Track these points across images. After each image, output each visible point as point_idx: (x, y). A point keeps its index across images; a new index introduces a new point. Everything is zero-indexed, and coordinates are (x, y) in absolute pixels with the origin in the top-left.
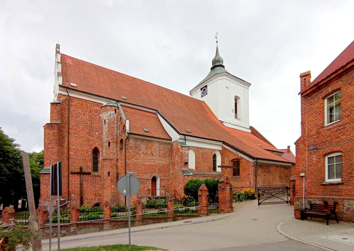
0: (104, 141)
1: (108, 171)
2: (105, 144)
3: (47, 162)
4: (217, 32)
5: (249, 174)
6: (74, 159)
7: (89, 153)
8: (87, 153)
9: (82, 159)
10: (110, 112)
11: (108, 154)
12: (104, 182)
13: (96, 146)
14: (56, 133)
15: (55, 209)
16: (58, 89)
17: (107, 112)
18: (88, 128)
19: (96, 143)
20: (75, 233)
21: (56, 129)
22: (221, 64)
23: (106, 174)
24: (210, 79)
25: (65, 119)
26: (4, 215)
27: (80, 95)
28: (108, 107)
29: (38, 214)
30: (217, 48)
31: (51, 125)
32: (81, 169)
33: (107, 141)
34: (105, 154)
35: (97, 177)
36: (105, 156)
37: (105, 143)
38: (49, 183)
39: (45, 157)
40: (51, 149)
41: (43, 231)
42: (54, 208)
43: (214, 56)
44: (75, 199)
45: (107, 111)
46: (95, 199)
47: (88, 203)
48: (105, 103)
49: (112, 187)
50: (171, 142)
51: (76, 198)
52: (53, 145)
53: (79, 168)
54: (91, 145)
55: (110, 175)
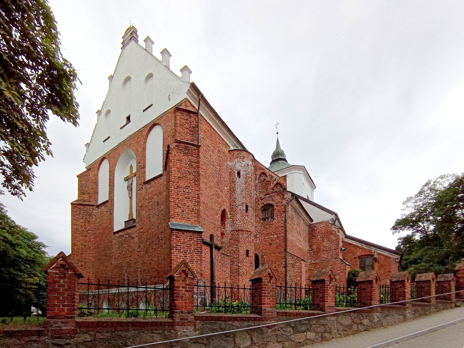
0: (238, 203)
1: (245, 249)
2: (239, 207)
3: (176, 210)
4: (277, 122)
5: (389, 272)
10: (247, 161)
12: (239, 264)
14: (195, 163)
16: (187, 90)
17: (244, 160)
19: (225, 203)
20: (380, 325)
21: (194, 155)
22: (281, 157)
23: (242, 252)
24: (283, 170)
26: (267, 283)
27: (211, 119)
28: (244, 153)
30: (278, 139)
31: (185, 147)
33: (242, 203)
34: (240, 222)
37: (239, 205)
38: (189, 249)
39: (173, 202)
40: (184, 188)
41: (336, 320)
43: (274, 149)
45: (242, 157)
50: (311, 223)
52: (190, 183)
53: (209, 236)
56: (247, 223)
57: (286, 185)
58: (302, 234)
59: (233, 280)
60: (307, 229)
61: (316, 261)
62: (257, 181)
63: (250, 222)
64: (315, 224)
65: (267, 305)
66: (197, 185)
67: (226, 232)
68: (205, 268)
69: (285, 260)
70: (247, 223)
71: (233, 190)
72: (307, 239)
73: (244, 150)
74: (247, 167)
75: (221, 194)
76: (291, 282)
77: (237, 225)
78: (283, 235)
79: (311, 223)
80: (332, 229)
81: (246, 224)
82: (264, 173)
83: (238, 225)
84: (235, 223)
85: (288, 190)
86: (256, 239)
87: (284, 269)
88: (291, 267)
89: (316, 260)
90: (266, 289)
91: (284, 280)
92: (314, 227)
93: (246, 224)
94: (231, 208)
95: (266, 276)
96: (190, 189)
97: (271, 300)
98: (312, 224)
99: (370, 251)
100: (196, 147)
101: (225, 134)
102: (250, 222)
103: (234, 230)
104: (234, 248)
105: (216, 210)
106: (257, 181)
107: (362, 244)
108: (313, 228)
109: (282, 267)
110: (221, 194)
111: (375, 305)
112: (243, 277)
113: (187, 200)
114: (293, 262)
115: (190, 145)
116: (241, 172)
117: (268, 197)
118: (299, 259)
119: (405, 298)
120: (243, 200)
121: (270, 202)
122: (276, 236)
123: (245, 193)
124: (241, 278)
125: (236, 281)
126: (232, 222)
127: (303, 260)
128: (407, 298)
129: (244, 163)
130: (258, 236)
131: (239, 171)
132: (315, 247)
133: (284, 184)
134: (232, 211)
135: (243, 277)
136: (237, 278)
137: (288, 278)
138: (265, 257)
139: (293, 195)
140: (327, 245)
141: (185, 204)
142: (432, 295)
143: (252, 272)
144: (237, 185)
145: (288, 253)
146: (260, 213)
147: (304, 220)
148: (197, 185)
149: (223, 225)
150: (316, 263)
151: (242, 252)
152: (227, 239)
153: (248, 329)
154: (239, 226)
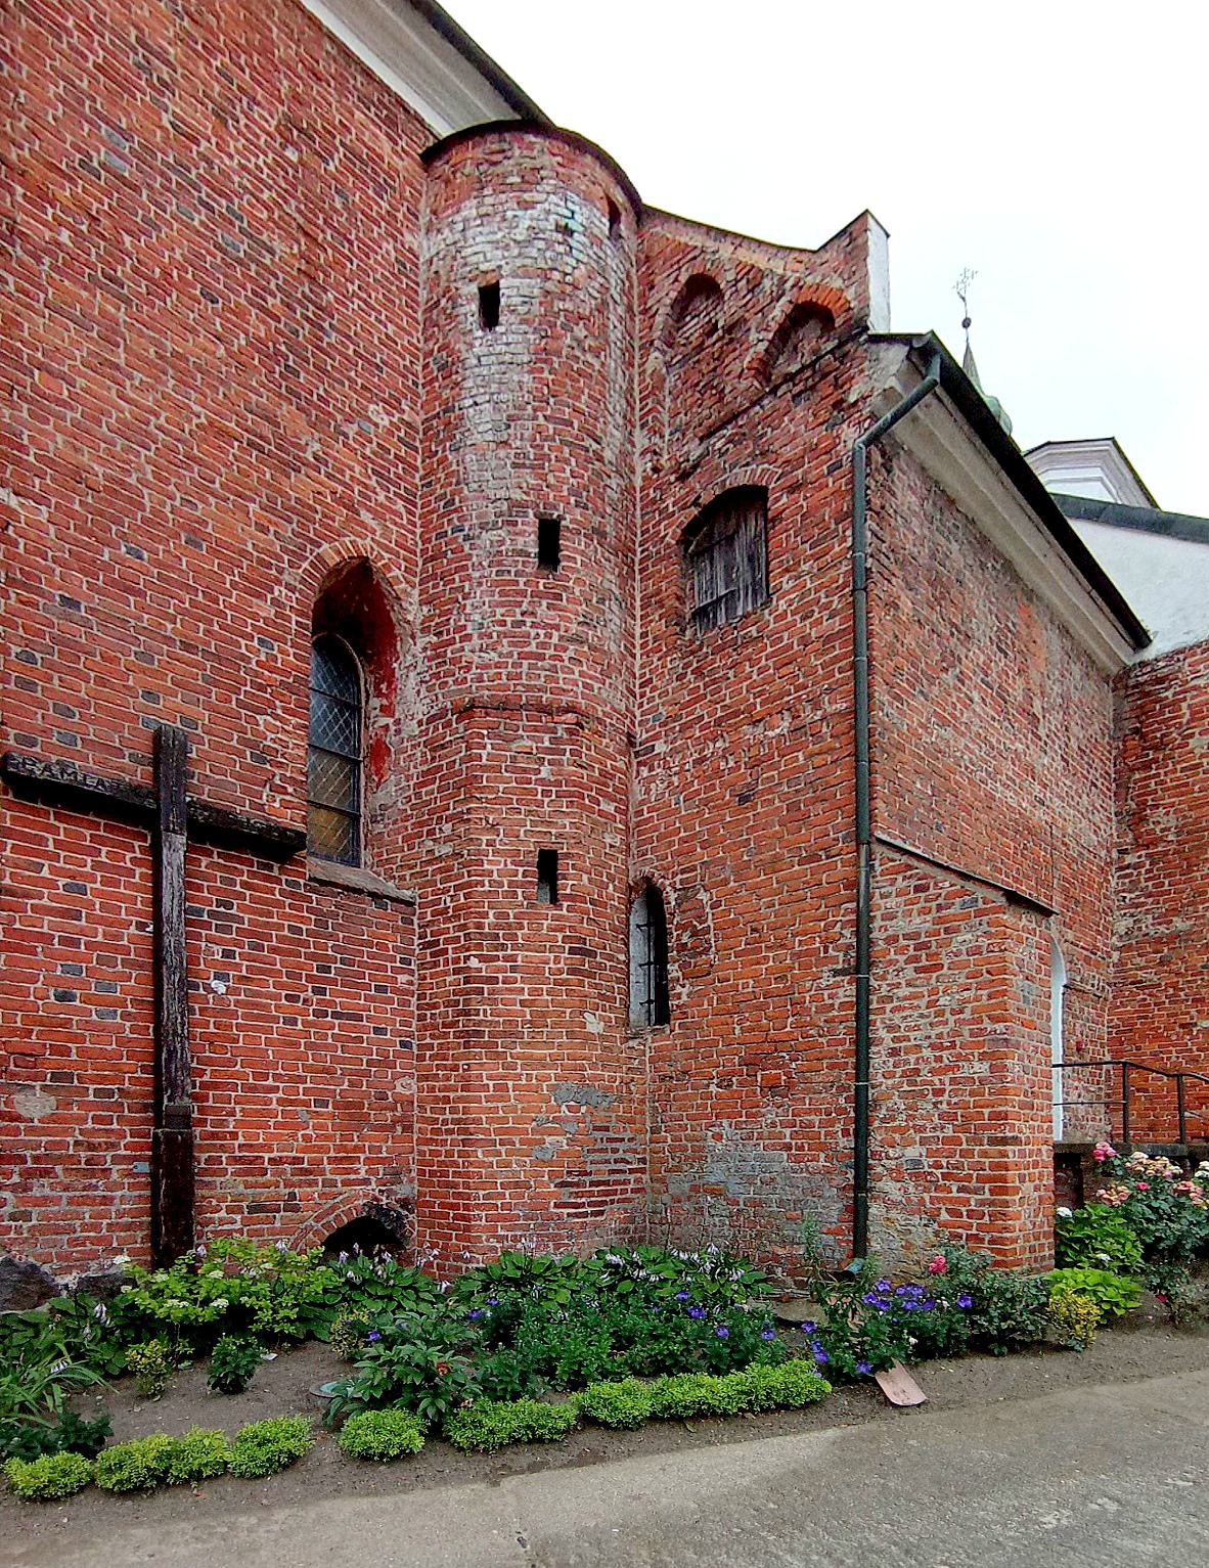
0: (475, 509)
1: (530, 846)
8: (259, 587)
9: (186, 647)
11: (533, 648)
12: (474, 963)
13: (366, 545)
17: (526, 196)
19: (366, 516)
30: (968, 347)
32: (165, 751)
35: (372, 907)
44: (60, 1160)
46: (345, 1160)
47: (252, 1209)
49: (590, 1028)
51: (91, 1147)
54: (303, 511)
55: (566, 886)
57: (864, 298)
58: (1050, 724)
60: (1105, 701)
61: (1179, 924)
62: (655, 359)
63: (579, 640)
64: (1169, 657)
67: (398, 732)
69: (857, 911)
72: (1102, 765)
73: (527, 120)
74: (550, 244)
76: (904, 1095)
77: (468, 669)
78: (842, 706)
79: (1129, 658)
81: (542, 657)
82: (702, 287)
84: (453, 661)
85: (877, 327)
86: (645, 772)
87: (847, 991)
88: (910, 972)
89: (1175, 912)
91: (846, 1075)
92: (1160, 681)
94: (433, 558)
98: (1143, 664)
101: (381, 24)
104: (448, 840)
106: (655, 359)
108: (1148, 694)
109: (836, 973)
114: (920, 923)
116: (503, 283)
118: (981, 892)
120: (516, 485)
121: (741, 477)
122: (784, 725)
124: (486, 1073)
126: (437, 653)
127: (1014, 899)
129: (526, 219)
130: (660, 747)
131: (491, 279)
132: (1163, 821)
133: (850, 294)
134: (434, 576)
136: (455, 1068)
137: (879, 1059)
138: (703, 896)
139: (924, 350)
145: (878, 849)
146: (668, 576)
147: (1065, 631)
149: (383, 686)
150: (1175, 936)
151: (495, 865)
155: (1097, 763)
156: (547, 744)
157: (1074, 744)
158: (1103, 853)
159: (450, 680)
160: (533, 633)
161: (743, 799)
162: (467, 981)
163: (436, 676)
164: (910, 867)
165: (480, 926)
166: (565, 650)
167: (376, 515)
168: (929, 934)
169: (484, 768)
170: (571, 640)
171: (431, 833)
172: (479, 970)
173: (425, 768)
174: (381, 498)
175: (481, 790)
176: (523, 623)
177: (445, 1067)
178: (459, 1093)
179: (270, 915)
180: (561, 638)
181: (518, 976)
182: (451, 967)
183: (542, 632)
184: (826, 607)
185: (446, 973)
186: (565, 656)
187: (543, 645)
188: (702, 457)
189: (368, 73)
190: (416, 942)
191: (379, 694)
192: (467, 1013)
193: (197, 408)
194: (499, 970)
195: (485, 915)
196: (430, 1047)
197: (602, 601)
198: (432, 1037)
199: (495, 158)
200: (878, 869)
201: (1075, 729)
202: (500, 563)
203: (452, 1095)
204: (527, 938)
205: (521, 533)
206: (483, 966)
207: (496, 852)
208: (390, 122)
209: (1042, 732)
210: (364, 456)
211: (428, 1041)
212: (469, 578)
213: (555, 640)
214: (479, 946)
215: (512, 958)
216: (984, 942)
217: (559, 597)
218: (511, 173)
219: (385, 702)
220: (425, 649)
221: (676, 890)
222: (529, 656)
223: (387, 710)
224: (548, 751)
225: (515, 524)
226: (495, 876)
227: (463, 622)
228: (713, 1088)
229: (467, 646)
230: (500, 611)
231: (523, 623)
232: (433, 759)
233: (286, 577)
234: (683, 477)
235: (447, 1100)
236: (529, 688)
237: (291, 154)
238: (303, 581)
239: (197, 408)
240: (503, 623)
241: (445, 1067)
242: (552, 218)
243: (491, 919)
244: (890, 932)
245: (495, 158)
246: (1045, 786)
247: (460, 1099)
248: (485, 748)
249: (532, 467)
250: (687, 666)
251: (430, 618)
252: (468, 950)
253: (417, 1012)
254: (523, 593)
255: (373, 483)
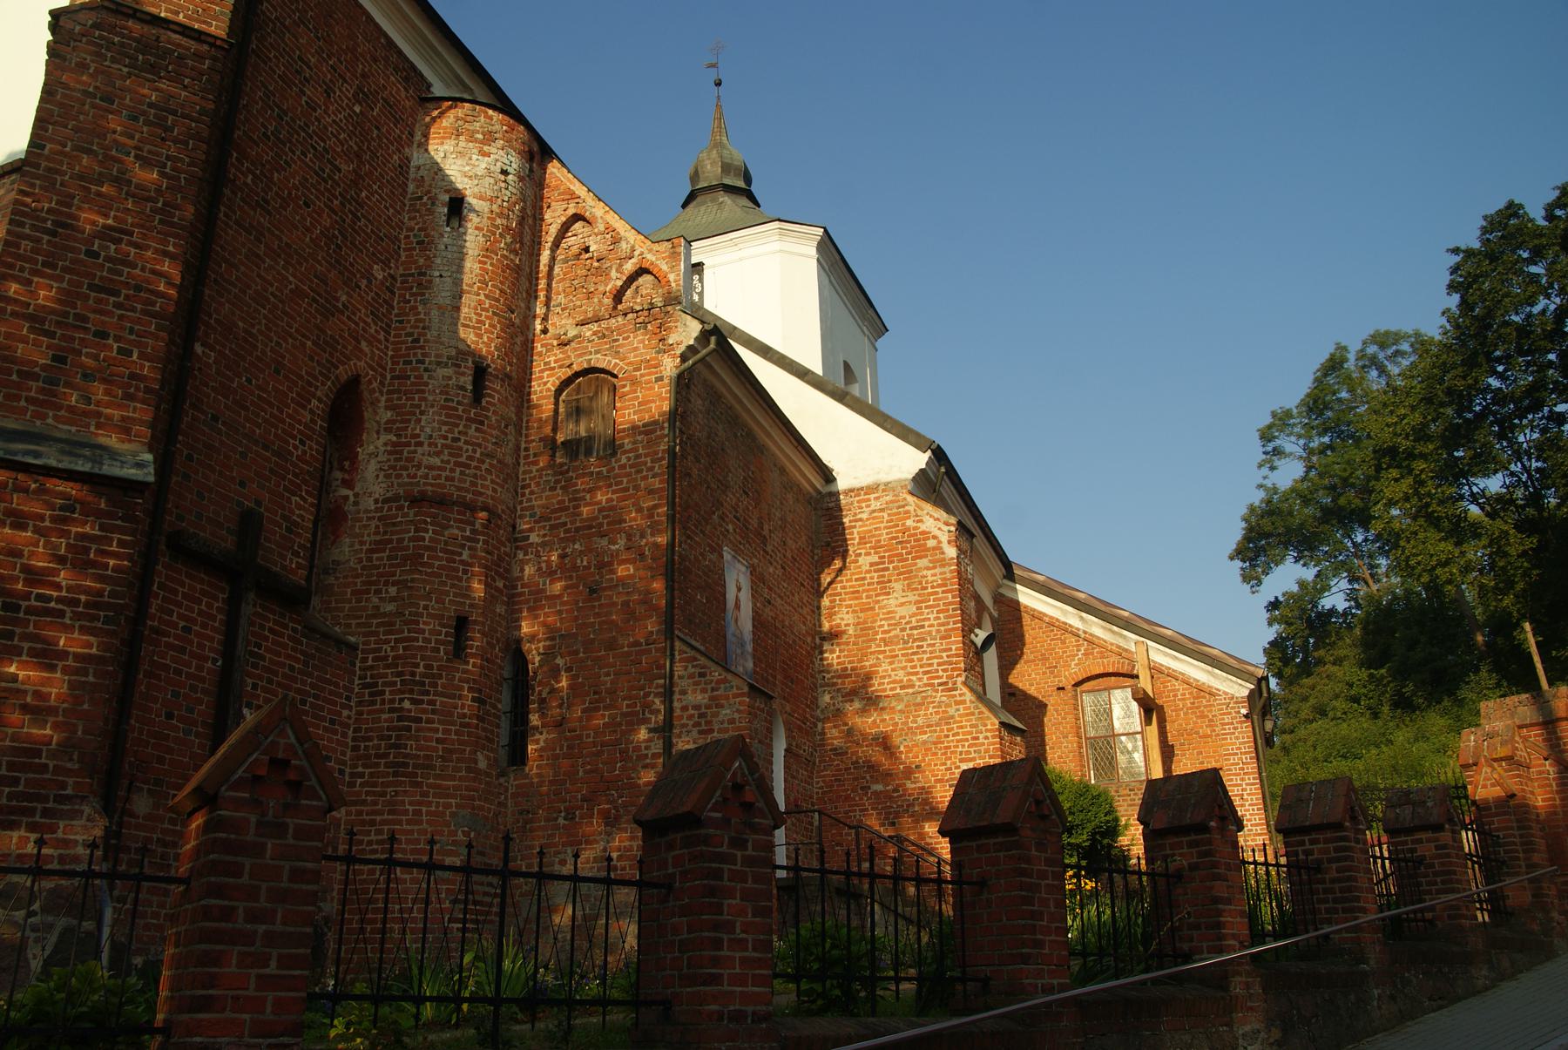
1: (452, 611)
2: (442, 372)
6: (215, 419)
7: (312, 411)
10: (501, 152)
11: (463, 459)
12: (407, 704)
14: (184, 116)
15: (67, 931)
18: (335, 202)
19: (364, 345)
25: (65, 86)
29: (722, 858)
34: (438, 454)
36: (430, 468)
37: (439, 364)
42: (62, 922)
48: (448, 86)
56: (474, 464)
59: (364, 802)
65: (228, 1014)
66: (172, 225)
68: (170, 716)
70: (474, 464)
71: (420, 284)
75: (344, 298)
77: (419, 467)
79: (824, 490)
80: (923, 527)
81: (468, 466)
83: (423, 471)
84: (410, 460)
90: (245, 879)
93: (468, 466)
94: (398, 377)
95: (257, 779)
96: (130, 243)
97: (272, 969)
99: (1121, 652)
100: (206, 47)
102: (490, 456)
103: (396, 498)
104: (393, 600)
105: (301, 377)
107: (1084, 615)
110: (344, 298)
111: (1049, 990)
112: (419, 785)
113: (99, 301)
114: (699, 698)
115: (175, 32)
117: (595, 333)
119: (1221, 938)
121: (601, 361)
123: (480, 303)
125: (380, 813)
126: (396, 449)
128: (1234, 937)
135: (419, 785)
136: (384, 794)
140: (902, 611)
141: (85, 319)
142: (1364, 911)
143: (480, 756)
144: (438, 261)
148: (172, 225)
151: (427, 625)
152: (357, 547)
153: (989, 1017)
154: (426, 477)
155: (804, 568)
156: (468, 533)
157: (789, 555)
158: (809, 640)
159: (404, 473)
160: (465, 447)
161: (592, 591)
162: (400, 719)
163: (393, 468)
164: (695, 659)
165: (413, 674)
166: (483, 462)
167: (370, 343)
168: (708, 707)
169: (427, 548)
170: (487, 455)
171: (378, 592)
172: (409, 711)
173: (378, 538)
174: (373, 331)
175: (424, 565)
176: (459, 439)
177: (374, 794)
178: (386, 817)
179: (1337, 850)
180: (482, 454)
181: (436, 717)
182: (387, 706)
183: (470, 448)
184: (652, 469)
185: (382, 711)
186: (483, 467)
187: (471, 458)
188: (576, 337)
189: (400, 53)
190: (357, 682)
191: (342, 469)
192: (397, 746)
193: (291, 279)
194: (424, 711)
195: (417, 666)
196: (362, 775)
197: (506, 427)
198: (365, 766)
199: (469, 118)
200: (677, 657)
201: (790, 542)
202: (447, 393)
203: (378, 818)
204: (443, 686)
205: (463, 374)
206: (413, 707)
207: (429, 615)
208: (406, 79)
209: (769, 548)
210: (368, 302)
211: (360, 769)
212: (425, 399)
213: (478, 455)
214: (411, 691)
215: (432, 703)
216: (736, 716)
217: (482, 423)
218: (478, 132)
219: (346, 476)
220: (385, 444)
221: (539, 654)
222: (457, 464)
223: (348, 484)
224: (468, 539)
225: (459, 366)
226: (427, 635)
227: (417, 431)
228: (561, 821)
229: (420, 450)
230: (444, 428)
231: (459, 439)
232: (385, 533)
233: (319, 393)
234: (563, 344)
235: (373, 823)
236: (459, 489)
237: (357, 109)
238: (327, 396)
239: (291, 279)
240: (445, 438)
241: (374, 794)
242: (499, 164)
243: (421, 669)
244: (684, 703)
245: (469, 118)
246: (771, 589)
247: (384, 822)
248: (427, 531)
249: (474, 328)
250: (557, 482)
251: (394, 422)
252: (403, 693)
253: (351, 744)
254: (460, 418)
255: (369, 320)
